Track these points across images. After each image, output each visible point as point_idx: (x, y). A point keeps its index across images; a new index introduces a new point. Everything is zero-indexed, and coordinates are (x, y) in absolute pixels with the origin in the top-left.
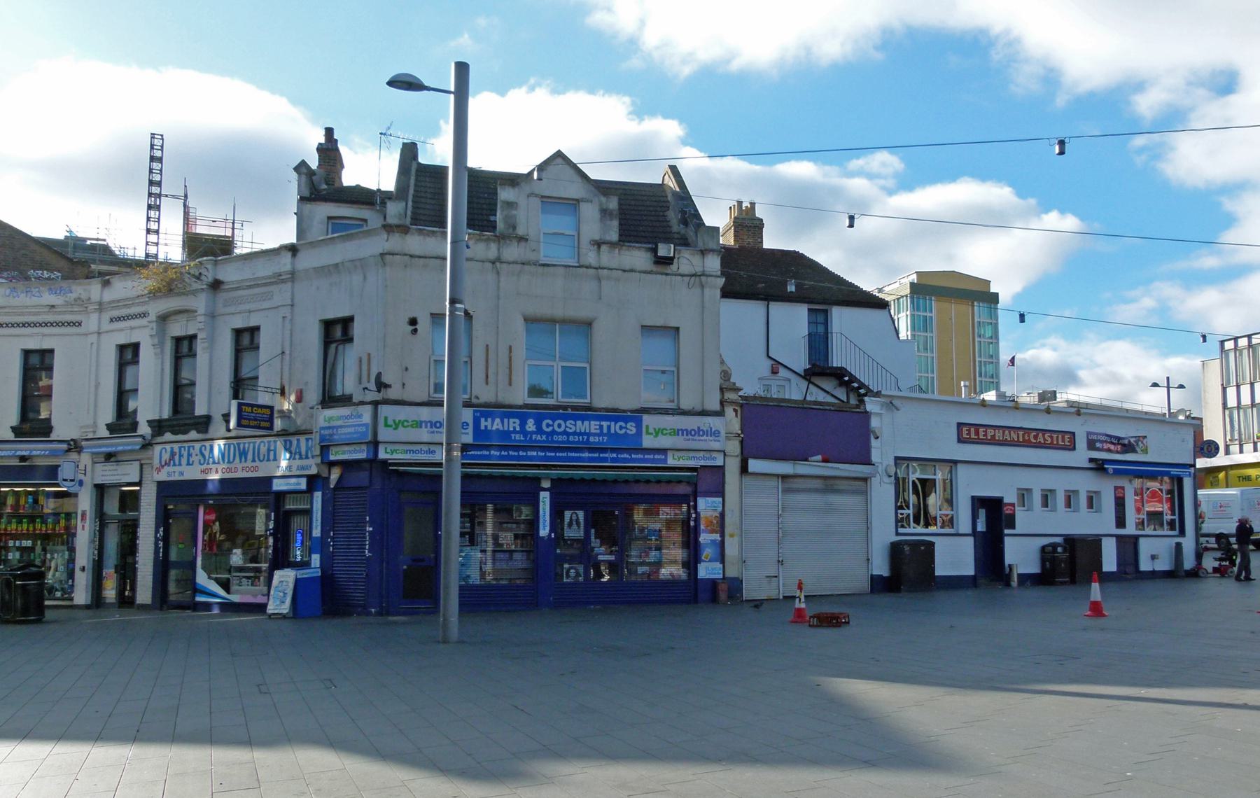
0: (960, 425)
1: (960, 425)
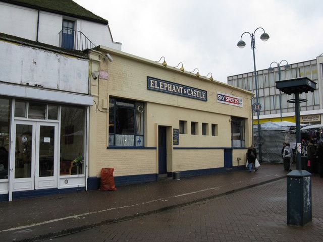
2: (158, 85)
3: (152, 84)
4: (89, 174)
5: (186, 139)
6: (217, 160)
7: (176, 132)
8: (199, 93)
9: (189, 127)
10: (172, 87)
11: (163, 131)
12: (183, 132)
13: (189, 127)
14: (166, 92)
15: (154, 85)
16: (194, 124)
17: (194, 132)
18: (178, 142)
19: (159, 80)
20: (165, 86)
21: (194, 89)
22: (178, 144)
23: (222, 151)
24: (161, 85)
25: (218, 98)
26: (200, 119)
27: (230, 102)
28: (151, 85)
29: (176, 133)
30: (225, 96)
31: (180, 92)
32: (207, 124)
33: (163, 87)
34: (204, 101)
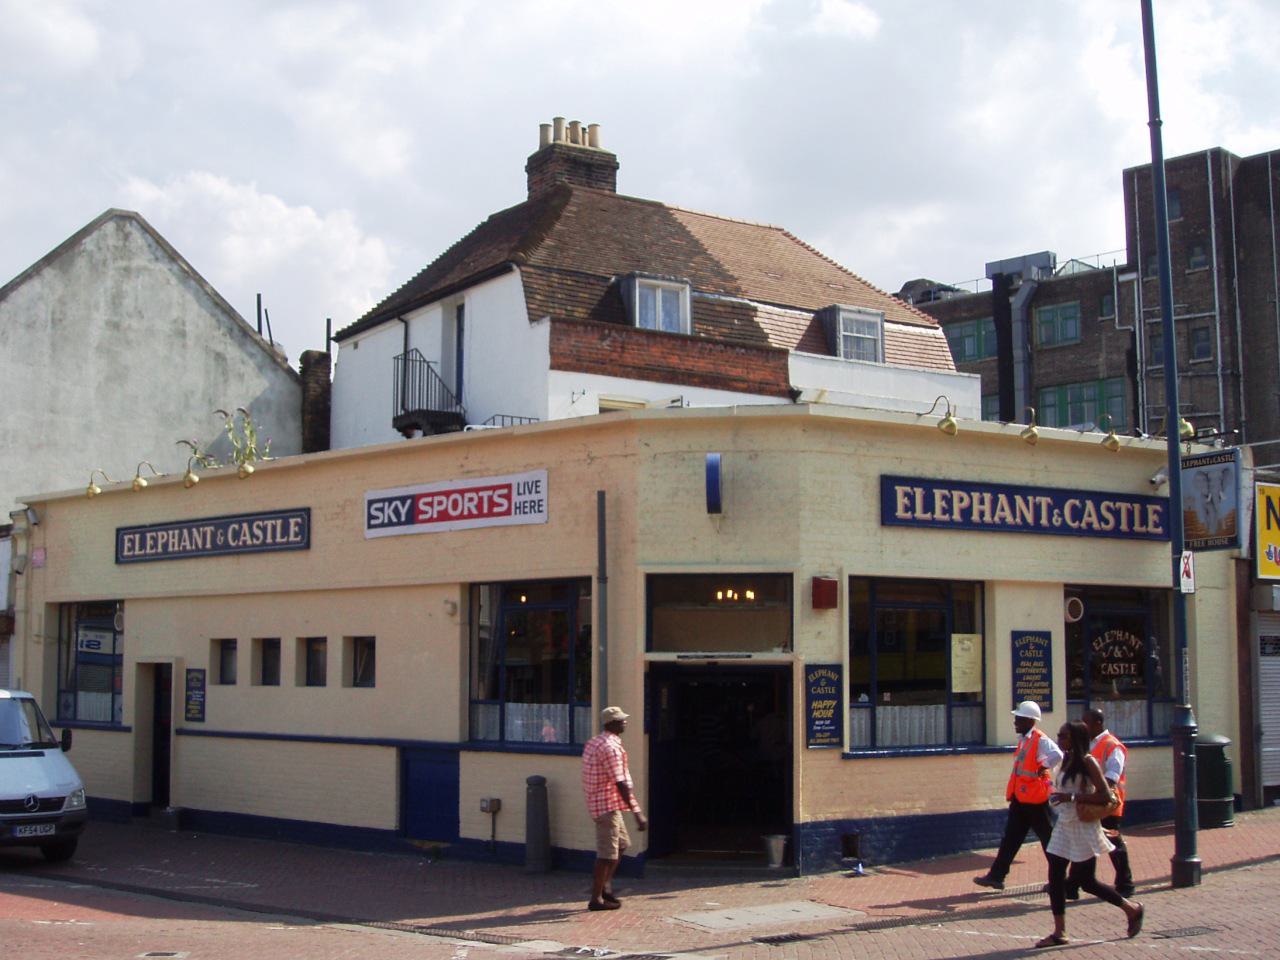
0: (888, 484)
1: (888, 484)
2: (929, 506)
3: (127, 544)
4: (27, 745)
5: (227, 705)
6: (370, 797)
7: (830, 682)
8: (274, 528)
9: (245, 661)
10: (994, 502)
11: (159, 674)
12: (226, 677)
13: (245, 661)
14: (966, 524)
15: (911, 508)
16: (269, 649)
17: (269, 674)
18: (202, 711)
19: (929, 485)
20: (956, 506)
21: (250, 518)
22: (202, 720)
23: (389, 759)
24: (939, 504)
25: (371, 517)
26: (290, 627)
27: (444, 516)
28: (126, 548)
29: (196, 681)
30: (415, 499)
31: (204, 543)
32: (324, 640)
33: (948, 510)
34: (300, 549)
